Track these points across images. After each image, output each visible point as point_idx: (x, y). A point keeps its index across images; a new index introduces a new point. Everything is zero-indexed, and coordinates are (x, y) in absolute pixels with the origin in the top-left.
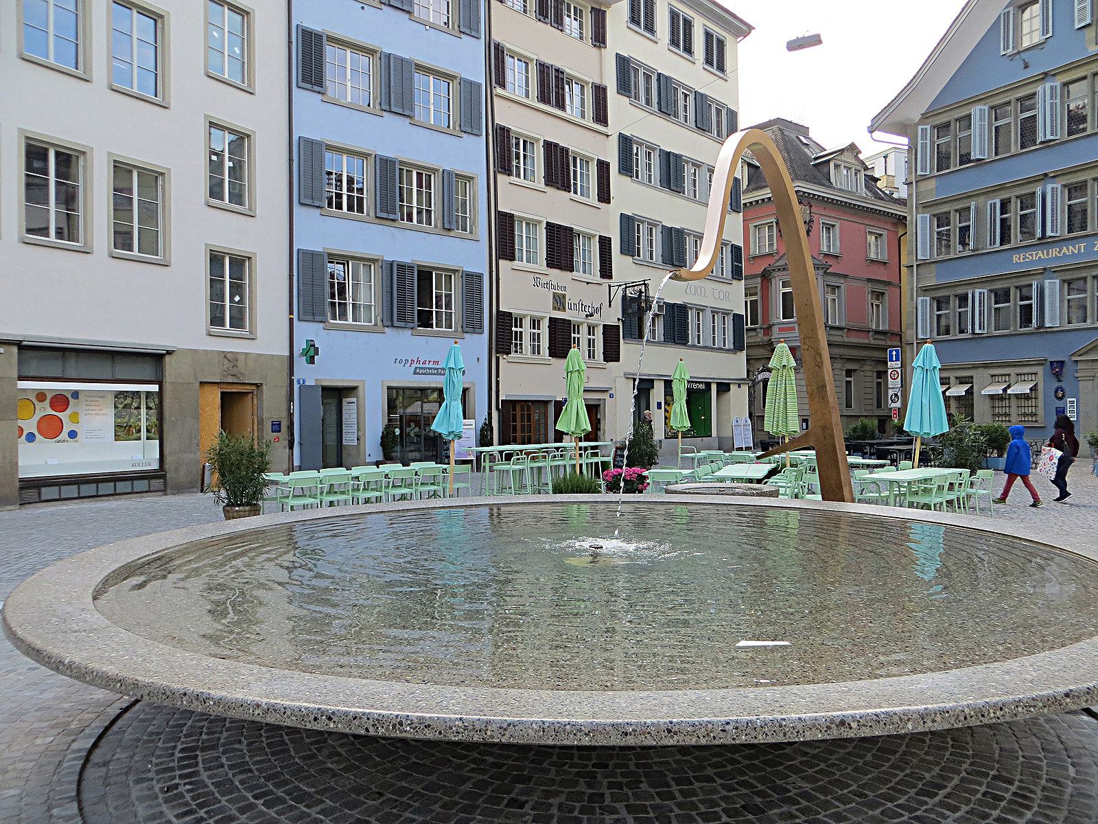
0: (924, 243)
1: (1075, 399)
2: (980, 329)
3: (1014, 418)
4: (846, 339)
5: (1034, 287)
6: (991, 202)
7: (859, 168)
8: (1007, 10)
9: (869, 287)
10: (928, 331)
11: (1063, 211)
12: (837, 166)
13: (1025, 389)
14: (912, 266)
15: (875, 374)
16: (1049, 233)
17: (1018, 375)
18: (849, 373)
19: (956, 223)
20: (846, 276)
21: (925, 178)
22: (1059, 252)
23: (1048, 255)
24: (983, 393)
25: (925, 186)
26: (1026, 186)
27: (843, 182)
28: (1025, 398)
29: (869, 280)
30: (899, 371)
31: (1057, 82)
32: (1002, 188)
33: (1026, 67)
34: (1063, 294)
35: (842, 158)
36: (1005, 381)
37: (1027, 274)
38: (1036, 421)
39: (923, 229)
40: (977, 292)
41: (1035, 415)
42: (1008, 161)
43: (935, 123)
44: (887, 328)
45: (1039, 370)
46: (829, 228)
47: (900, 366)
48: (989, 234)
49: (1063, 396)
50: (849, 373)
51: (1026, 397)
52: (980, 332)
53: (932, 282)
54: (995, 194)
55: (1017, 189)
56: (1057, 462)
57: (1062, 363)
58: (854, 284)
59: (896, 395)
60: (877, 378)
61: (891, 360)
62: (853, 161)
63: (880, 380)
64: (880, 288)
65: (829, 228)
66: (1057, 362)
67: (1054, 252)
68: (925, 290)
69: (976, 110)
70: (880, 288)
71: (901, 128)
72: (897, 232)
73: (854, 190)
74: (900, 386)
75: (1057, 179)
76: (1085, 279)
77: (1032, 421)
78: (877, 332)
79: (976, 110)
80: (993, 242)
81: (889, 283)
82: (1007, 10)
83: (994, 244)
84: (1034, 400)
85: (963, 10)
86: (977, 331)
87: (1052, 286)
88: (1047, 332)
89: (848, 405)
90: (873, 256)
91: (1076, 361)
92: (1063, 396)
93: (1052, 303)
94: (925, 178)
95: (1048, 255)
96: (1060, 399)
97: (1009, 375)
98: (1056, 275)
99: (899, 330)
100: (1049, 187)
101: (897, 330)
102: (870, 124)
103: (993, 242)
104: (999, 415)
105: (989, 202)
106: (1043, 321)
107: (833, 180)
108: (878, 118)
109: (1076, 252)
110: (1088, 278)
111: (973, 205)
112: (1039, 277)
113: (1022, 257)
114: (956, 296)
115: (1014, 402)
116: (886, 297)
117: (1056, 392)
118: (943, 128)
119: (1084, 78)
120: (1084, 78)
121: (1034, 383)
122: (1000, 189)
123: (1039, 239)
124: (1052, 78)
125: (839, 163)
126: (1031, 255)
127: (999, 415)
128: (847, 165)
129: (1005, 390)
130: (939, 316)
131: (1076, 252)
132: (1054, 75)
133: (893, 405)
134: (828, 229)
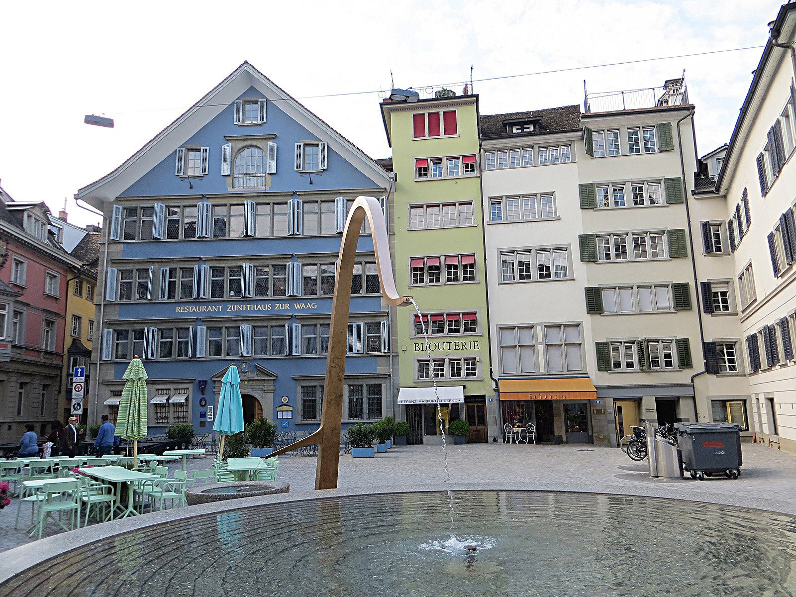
0: (111, 289)
1: (212, 406)
2: (151, 356)
3: (171, 420)
4: (24, 357)
5: (191, 330)
6: (163, 268)
7: (45, 222)
8: (181, 149)
9: (44, 316)
10: (110, 355)
11: (209, 283)
12: (29, 216)
13: (181, 399)
14: (101, 305)
15: (18, 385)
16: (202, 296)
17: (175, 389)
18: (22, 385)
19: (136, 279)
20: (27, 305)
21: (114, 242)
22: (206, 309)
23: (199, 310)
24: (152, 402)
25: (114, 248)
26: (187, 263)
27: (32, 231)
28: (179, 406)
29: (44, 310)
30: (83, 384)
31: (210, 203)
32: (171, 261)
33: (191, 188)
34: (114, 340)
35: (34, 211)
36: (166, 394)
37: (186, 321)
38: (186, 422)
39: (112, 278)
40: (151, 329)
41: (185, 417)
42: (222, 243)
43: (126, 206)
44: (54, 350)
45: (190, 386)
46: (18, 263)
47: (83, 380)
48: (160, 290)
49: (205, 404)
50: (22, 385)
51: (180, 405)
52: (151, 358)
53: (115, 318)
54: (166, 264)
55: (182, 263)
56: (50, 450)
57: (205, 382)
58: (34, 312)
59: (79, 404)
60: (43, 390)
61: (77, 376)
62: (41, 216)
63: (44, 392)
64: (51, 318)
65: (18, 263)
66: (203, 381)
67: (203, 308)
68: (109, 324)
69: (158, 205)
70: (51, 318)
71: (100, 204)
72: (66, 276)
73: (40, 238)
74: (82, 397)
75: (207, 262)
76: (315, 325)
77: (165, 422)
78: (47, 353)
79: (158, 205)
80: (163, 296)
81: (58, 315)
82: (181, 149)
83: (164, 297)
84: (167, 408)
85: (155, 138)
86: (150, 357)
87: (202, 330)
88: (196, 361)
89: (19, 413)
90: (47, 291)
91: (215, 381)
92: (205, 404)
93: (201, 341)
94: (114, 242)
95: (199, 310)
96: (203, 406)
97: (187, 389)
98: (203, 323)
99: (61, 352)
100: (203, 266)
101: (60, 352)
102: (77, 193)
103: (163, 296)
104: (160, 418)
105: (162, 269)
106: (196, 354)
107: (25, 226)
108: (83, 190)
109: (217, 310)
110: (130, 331)
111: (151, 268)
112: (194, 323)
113: (182, 309)
114: (133, 331)
115: (172, 409)
116: (56, 325)
117: (201, 401)
118: (132, 212)
119: (225, 205)
120: (225, 205)
121: (187, 395)
122: (169, 262)
123: (195, 299)
124: (298, 196)
125: (31, 214)
126: (189, 308)
127: (160, 418)
128: (37, 218)
129: (168, 400)
130: (117, 344)
131: (217, 310)
132: (208, 198)
133: (75, 412)
134: (17, 264)
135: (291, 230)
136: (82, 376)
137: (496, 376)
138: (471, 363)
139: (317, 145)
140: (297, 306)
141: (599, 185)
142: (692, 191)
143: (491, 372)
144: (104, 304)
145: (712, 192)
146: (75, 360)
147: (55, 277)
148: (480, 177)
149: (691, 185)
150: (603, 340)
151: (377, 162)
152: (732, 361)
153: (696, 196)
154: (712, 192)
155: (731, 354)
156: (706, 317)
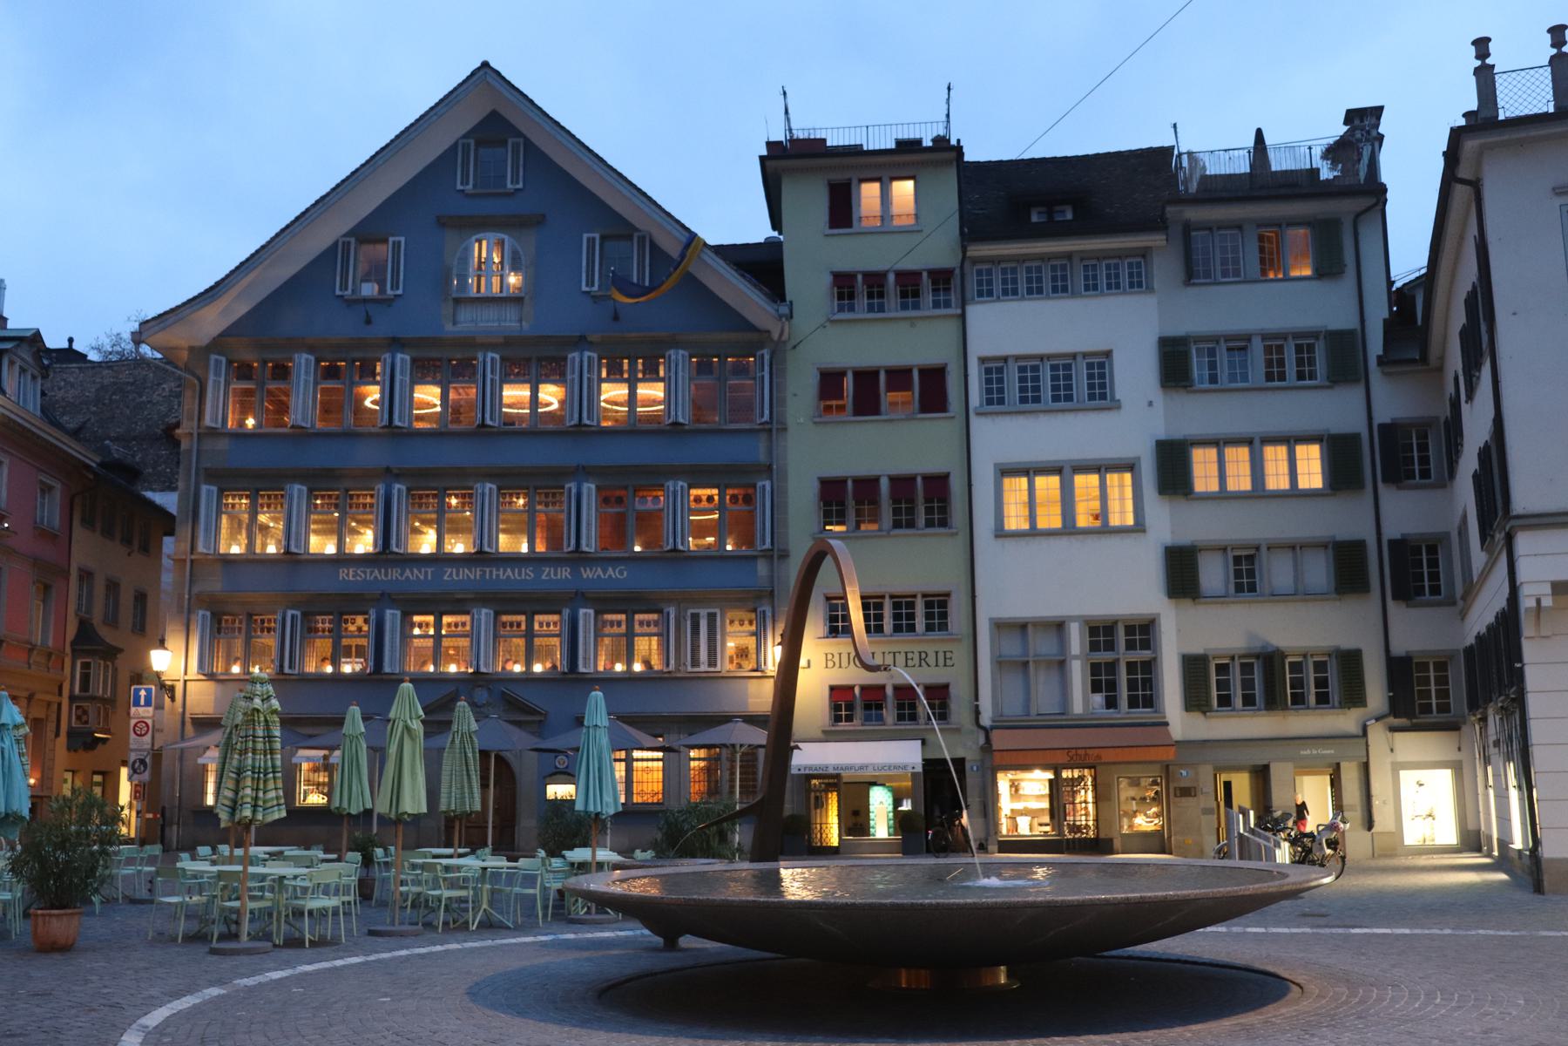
59: (142, 762)
61: (137, 704)
135: (576, 416)
136: (148, 704)
137: (986, 720)
138: (939, 694)
139: (630, 237)
140: (587, 574)
141: (1199, 339)
142: (1379, 357)
143: (977, 712)
144: (1241, 858)
145: (1413, 361)
146: (86, 666)
147: (51, 488)
148: (963, 317)
149: (1376, 346)
150: (1196, 649)
151: (720, 250)
152: (1434, 576)
153: (1387, 370)
154: (1413, 361)
155: (1433, 563)
156: (1396, 610)
